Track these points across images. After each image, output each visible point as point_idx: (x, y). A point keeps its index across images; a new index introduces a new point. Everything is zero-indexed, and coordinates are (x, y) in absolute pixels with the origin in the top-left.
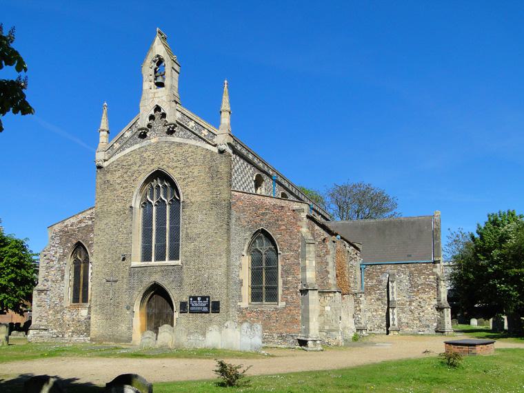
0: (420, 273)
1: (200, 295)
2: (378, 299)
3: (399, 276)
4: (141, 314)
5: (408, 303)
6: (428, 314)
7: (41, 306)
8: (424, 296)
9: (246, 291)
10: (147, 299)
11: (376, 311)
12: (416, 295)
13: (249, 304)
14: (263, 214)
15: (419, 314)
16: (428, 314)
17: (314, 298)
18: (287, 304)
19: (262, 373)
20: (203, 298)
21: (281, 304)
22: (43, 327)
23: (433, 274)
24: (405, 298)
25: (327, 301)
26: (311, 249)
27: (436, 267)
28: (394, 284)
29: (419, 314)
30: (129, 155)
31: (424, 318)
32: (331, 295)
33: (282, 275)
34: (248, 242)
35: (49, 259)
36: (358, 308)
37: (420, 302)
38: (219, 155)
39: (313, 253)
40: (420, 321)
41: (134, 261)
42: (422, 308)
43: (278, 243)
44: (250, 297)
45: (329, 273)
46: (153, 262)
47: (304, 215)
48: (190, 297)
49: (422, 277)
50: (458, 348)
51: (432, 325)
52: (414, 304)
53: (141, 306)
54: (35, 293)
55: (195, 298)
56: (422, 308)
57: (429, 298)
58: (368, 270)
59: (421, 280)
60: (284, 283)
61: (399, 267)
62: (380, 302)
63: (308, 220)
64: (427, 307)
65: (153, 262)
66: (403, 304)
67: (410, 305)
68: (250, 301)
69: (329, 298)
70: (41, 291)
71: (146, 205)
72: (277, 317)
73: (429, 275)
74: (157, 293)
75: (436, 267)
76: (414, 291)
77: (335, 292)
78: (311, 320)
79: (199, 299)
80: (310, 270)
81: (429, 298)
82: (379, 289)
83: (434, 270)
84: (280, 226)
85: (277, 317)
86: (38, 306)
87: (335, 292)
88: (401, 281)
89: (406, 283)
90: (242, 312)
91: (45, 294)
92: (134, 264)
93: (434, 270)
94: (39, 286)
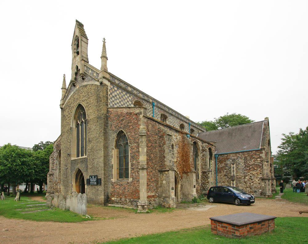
0: (252, 158)
1: (94, 175)
2: (225, 175)
3: (238, 160)
4: (76, 186)
5: (243, 177)
6: (256, 184)
7: (51, 182)
8: (254, 173)
9: (115, 172)
10: (79, 178)
11: (224, 182)
12: (248, 172)
13: (117, 180)
14: (122, 120)
15: (250, 184)
16: (256, 184)
17: (143, 174)
18: (133, 180)
19: (184, 211)
20: (95, 176)
21: (130, 180)
22: (52, 192)
23: (260, 157)
24: (241, 174)
25: (164, 177)
26: (143, 140)
27: (262, 153)
28: (235, 165)
29: (250, 184)
30: (70, 99)
31: (254, 187)
32: (166, 173)
33: (131, 160)
34: (115, 140)
35: (53, 159)
36: (207, 181)
37: (251, 176)
38: (100, 87)
39: (144, 142)
40: (251, 188)
41: (73, 157)
42: (252, 180)
43: (129, 138)
44: (118, 175)
45: (165, 158)
46: (80, 157)
47: (141, 116)
48: (90, 176)
49: (252, 160)
50: (222, 227)
51: (258, 191)
52: (247, 178)
53: (76, 182)
54: (48, 175)
55: (91, 176)
56: (252, 180)
57: (257, 174)
58: (220, 158)
59: (252, 162)
60: (132, 165)
61: (238, 155)
62: (226, 177)
63: (146, 120)
64: (255, 179)
65: (80, 157)
66: (240, 178)
67: (244, 178)
68: (118, 178)
69: (165, 175)
70: (50, 175)
71: (77, 125)
72: (128, 188)
73: (257, 159)
74: (79, 175)
75: (262, 153)
76: (247, 170)
77: (168, 171)
78: (141, 190)
79: (93, 177)
80: (142, 155)
81: (257, 174)
82: (226, 169)
83: (261, 155)
84: (130, 126)
85: (128, 188)
86: (50, 182)
87: (168, 171)
88: (239, 164)
89: (242, 165)
90: (113, 185)
91: (53, 176)
92: (73, 159)
93: (261, 155)
94: (50, 172)
